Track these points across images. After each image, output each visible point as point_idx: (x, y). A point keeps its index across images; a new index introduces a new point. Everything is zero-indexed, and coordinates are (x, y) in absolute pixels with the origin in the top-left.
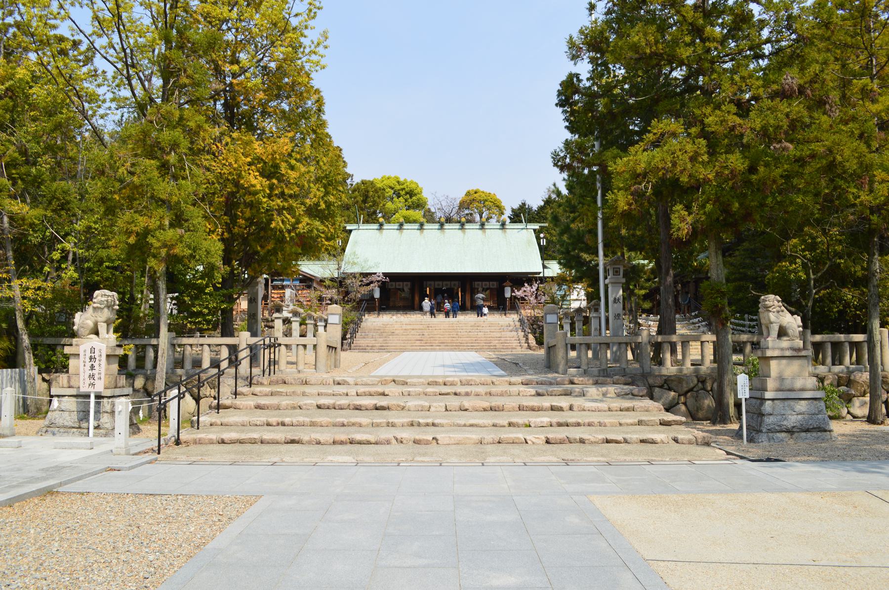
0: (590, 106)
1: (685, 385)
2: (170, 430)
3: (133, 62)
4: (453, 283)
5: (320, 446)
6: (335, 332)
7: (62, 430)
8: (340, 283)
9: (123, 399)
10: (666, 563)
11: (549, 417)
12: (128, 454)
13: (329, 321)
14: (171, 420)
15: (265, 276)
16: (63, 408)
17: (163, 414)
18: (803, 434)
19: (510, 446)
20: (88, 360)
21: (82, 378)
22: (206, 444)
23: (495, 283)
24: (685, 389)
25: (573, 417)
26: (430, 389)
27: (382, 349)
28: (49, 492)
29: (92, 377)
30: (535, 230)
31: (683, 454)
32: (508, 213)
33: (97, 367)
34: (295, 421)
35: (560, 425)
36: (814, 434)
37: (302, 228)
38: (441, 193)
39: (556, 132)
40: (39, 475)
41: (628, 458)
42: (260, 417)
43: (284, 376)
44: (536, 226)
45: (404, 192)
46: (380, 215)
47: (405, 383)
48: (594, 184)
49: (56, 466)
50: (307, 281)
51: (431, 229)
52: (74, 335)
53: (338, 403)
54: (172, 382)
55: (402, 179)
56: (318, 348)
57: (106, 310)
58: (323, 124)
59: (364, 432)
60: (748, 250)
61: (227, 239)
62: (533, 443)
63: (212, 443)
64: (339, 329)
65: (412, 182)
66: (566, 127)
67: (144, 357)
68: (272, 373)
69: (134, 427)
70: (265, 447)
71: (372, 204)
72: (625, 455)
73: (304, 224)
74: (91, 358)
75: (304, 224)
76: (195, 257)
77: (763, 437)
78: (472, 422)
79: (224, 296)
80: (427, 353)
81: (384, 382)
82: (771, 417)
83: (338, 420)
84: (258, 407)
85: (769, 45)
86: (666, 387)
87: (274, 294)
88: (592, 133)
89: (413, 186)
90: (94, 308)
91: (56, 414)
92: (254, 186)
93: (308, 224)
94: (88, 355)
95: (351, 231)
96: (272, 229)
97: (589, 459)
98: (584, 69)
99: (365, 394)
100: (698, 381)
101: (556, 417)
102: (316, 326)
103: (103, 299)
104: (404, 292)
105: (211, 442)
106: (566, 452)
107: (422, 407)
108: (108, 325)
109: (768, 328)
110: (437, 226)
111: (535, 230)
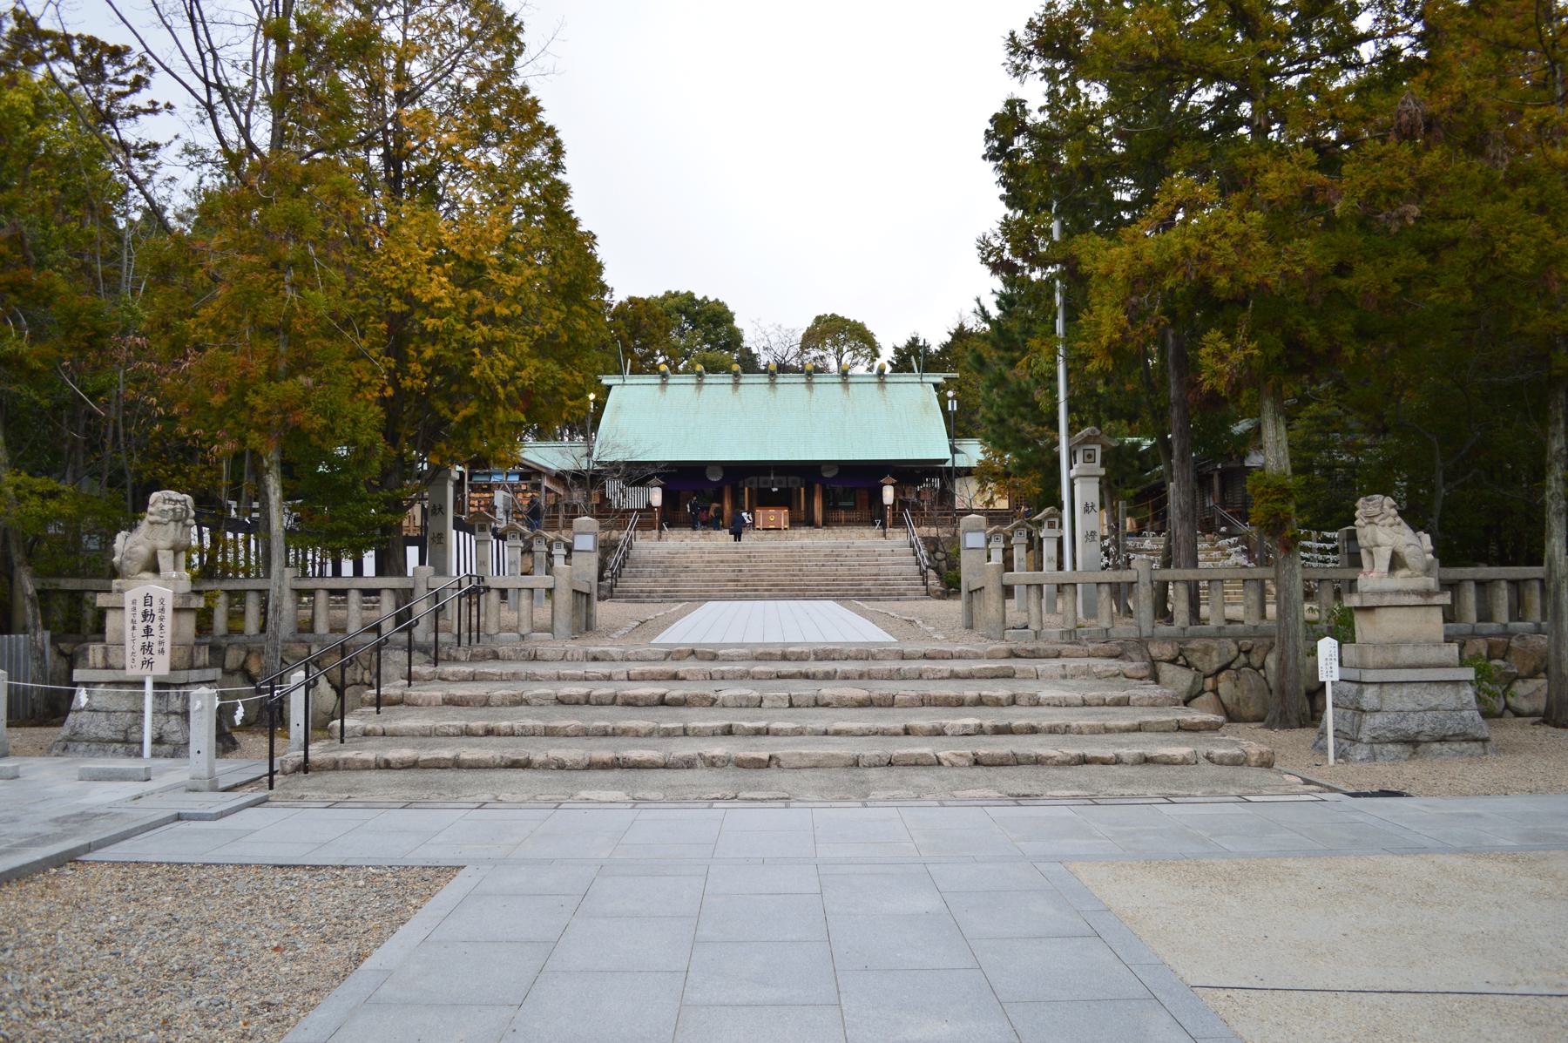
0: (1045, 155)
1: (1215, 659)
2: (291, 753)
3: (217, 78)
4: (791, 478)
5: (565, 773)
6: (587, 566)
7: (93, 746)
8: (590, 480)
9: (204, 690)
10: (1229, 992)
11: (977, 717)
12: (214, 789)
13: (576, 547)
14: (293, 725)
15: (459, 468)
16: (95, 705)
17: (277, 714)
18: (1436, 746)
19: (907, 770)
20: (139, 618)
21: (128, 651)
22: (357, 769)
24: (1216, 666)
25: (1021, 717)
26: (760, 668)
27: (670, 596)
28: (69, 859)
29: (147, 648)
30: (936, 386)
31: (1226, 783)
32: (887, 355)
33: (156, 631)
34: (517, 725)
35: (998, 731)
36: (1456, 746)
37: (527, 375)
38: (767, 324)
39: (984, 204)
40: (49, 829)
41: (1127, 792)
42: (454, 720)
43: (494, 646)
44: (939, 378)
46: (661, 359)
47: (714, 657)
48: (1051, 297)
49: (82, 814)
50: (531, 474)
51: (754, 386)
52: (115, 573)
53: (595, 693)
54: (293, 658)
56: (557, 595)
57: (172, 524)
58: (562, 191)
59: (644, 747)
60: (1316, 418)
61: (392, 399)
62: (953, 765)
63: (369, 768)
64: (594, 559)
66: (1002, 198)
67: (243, 613)
68: (474, 641)
69: (226, 741)
70: (466, 776)
72: (1122, 786)
73: (530, 369)
74: (145, 615)
75: (530, 369)
76: (332, 431)
77: (1361, 752)
78: (840, 725)
79: (387, 501)
81: (671, 655)
82: (1378, 716)
83: (597, 724)
84: (450, 702)
85: (1371, 43)
86: (1181, 660)
87: (474, 500)
88: (1049, 208)
90: (152, 523)
91: (84, 717)
92: (440, 300)
93: (537, 370)
94: (140, 608)
95: (609, 387)
96: (473, 380)
97: (1055, 793)
98: (1034, 92)
99: (643, 677)
100: (1240, 651)
101: (990, 717)
102: (550, 555)
103: (167, 507)
104: (703, 493)
105: (365, 766)
106: (1016, 779)
107: (749, 699)
108: (176, 554)
109: (1371, 553)
110: (764, 379)
111: (936, 386)
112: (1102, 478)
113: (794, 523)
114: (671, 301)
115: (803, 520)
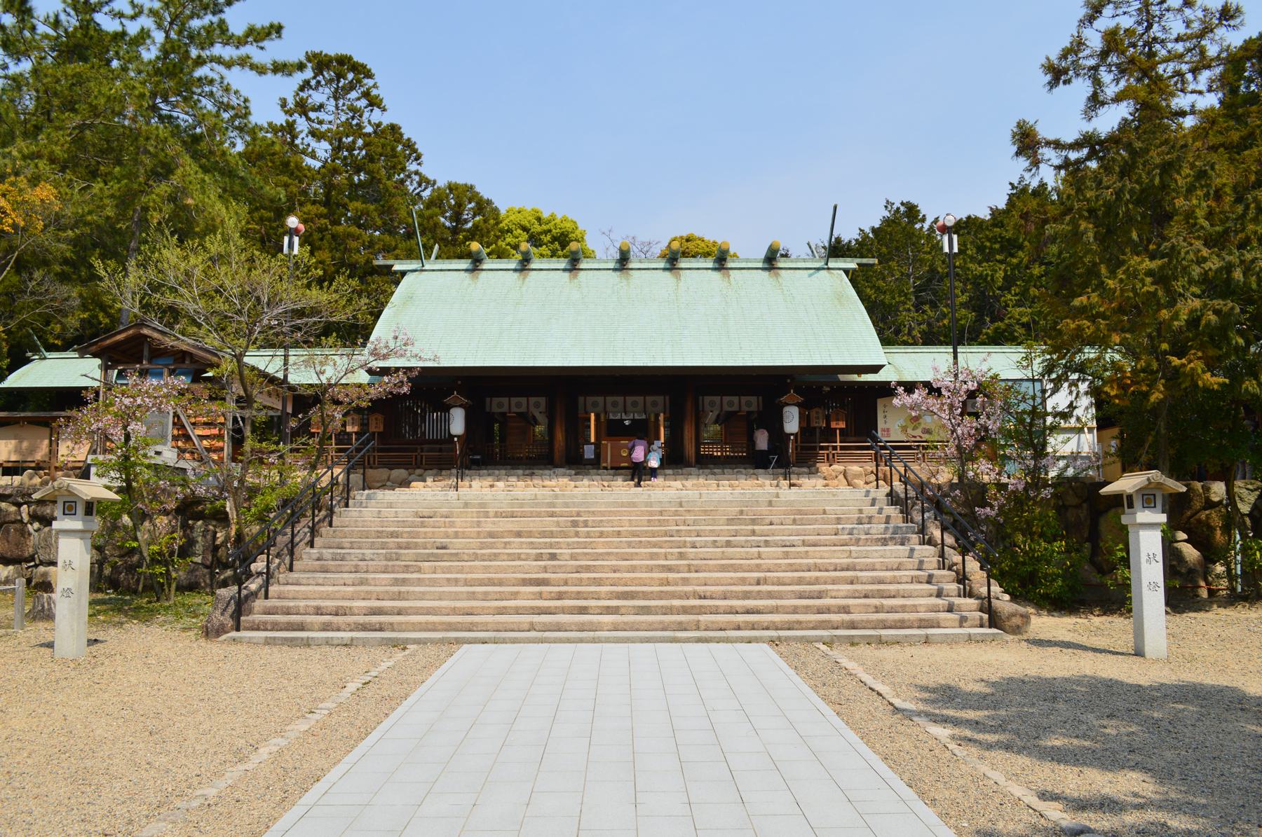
23: (753, 399)
45: (548, 238)
55: (545, 215)
65: (564, 220)
71: (466, 230)
80: (561, 653)
89: (568, 225)
95: (403, 273)
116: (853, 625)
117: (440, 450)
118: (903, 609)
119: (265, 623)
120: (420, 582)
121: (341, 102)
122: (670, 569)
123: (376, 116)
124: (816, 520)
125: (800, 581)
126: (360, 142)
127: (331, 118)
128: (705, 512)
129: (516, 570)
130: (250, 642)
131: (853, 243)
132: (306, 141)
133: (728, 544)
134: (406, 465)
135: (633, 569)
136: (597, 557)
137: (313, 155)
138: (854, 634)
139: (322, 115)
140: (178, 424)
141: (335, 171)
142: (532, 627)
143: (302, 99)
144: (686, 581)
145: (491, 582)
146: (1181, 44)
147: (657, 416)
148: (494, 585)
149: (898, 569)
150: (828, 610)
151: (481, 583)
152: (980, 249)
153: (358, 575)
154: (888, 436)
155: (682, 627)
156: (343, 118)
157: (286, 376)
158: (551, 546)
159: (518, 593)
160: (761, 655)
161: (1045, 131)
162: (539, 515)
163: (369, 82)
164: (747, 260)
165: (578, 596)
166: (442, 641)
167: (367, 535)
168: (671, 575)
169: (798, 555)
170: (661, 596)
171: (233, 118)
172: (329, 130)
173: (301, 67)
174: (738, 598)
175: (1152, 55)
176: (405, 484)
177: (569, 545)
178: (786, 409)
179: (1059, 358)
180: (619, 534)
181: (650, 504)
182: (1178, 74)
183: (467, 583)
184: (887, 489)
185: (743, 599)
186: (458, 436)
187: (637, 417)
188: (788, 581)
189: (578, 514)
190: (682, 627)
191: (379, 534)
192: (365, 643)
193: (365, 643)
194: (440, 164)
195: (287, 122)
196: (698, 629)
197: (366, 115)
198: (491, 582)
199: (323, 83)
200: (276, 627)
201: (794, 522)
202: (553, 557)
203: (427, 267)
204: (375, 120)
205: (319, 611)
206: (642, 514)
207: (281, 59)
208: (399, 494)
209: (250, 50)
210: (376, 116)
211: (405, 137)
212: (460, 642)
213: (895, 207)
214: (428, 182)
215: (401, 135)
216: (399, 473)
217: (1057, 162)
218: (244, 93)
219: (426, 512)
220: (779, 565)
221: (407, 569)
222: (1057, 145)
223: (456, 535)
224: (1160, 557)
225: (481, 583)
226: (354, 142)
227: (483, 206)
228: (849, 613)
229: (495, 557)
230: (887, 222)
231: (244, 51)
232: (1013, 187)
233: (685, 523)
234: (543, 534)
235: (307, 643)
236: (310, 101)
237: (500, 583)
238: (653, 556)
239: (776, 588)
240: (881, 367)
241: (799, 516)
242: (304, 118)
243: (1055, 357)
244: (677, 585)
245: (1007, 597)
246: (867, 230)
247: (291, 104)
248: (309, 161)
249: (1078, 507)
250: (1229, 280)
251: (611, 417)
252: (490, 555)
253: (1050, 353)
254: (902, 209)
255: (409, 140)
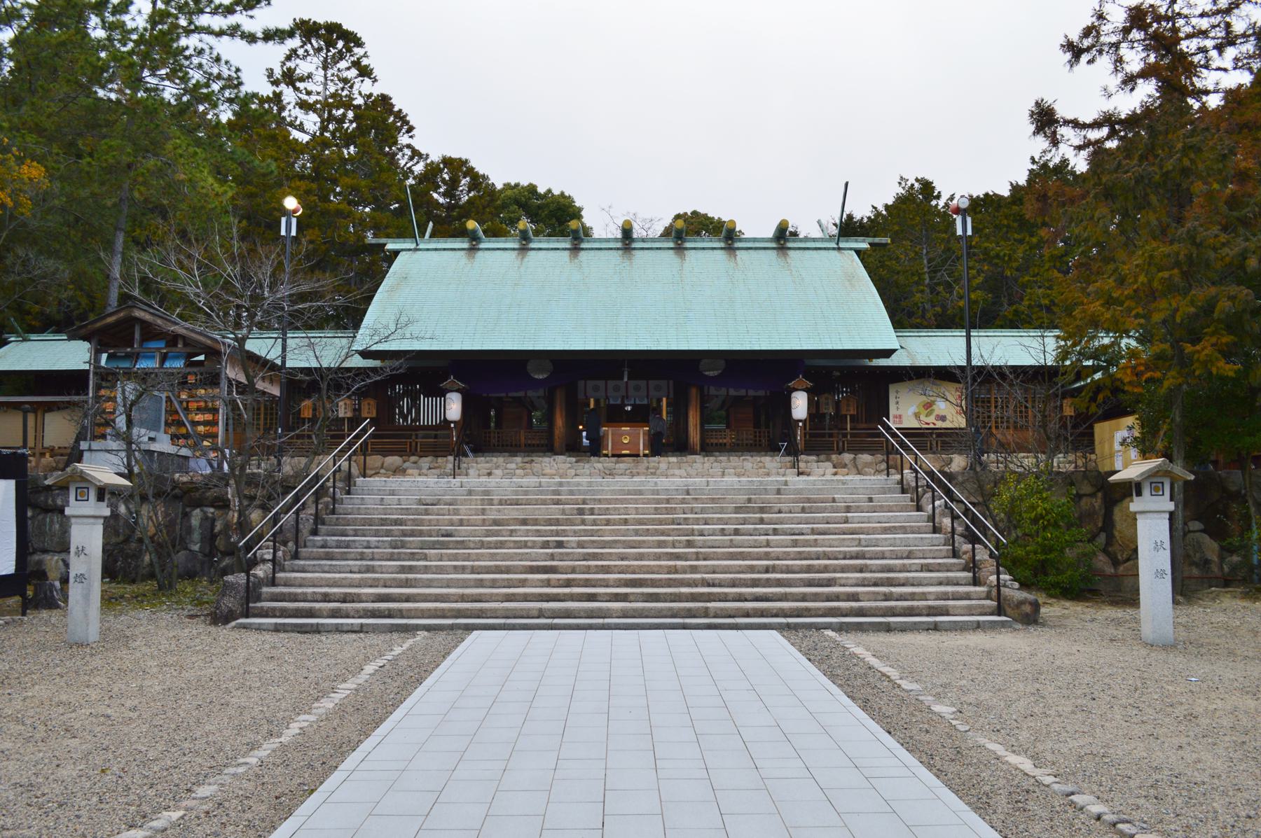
95: (396, 253)
112: (1171, 514)
113: (658, 447)
114: (509, 193)
115: (670, 443)
116: (861, 612)
117: (436, 437)
118: (912, 597)
119: (274, 609)
120: (426, 569)
121: (330, 72)
122: (677, 557)
123: (366, 87)
124: (825, 508)
125: (809, 569)
126: (350, 114)
127: (320, 89)
128: (713, 500)
129: (522, 557)
130: (259, 628)
131: (865, 220)
132: (294, 113)
133: (737, 532)
134: (400, 452)
135: (641, 557)
136: (604, 545)
137: (301, 128)
138: (860, 620)
139: (310, 86)
140: (172, 411)
141: (325, 144)
142: (541, 614)
143: (289, 69)
144: (694, 569)
145: (498, 570)
146: (1205, 19)
147: (659, 401)
148: (501, 572)
149: (908, 558)
150: (837, 598)
151: (488, 570)
152: (998, 227)
153: (365, 563)
154: (901, 422)
155: (691, 614)
156: (332, 89)
157: (284, 362)
158: (557, 534)
159: (526, 580)
160: (771, 645)
161: (1062, 112)
162: (544, 502)
163: (358, 51)
164: (755, 240)
165: (587, 583)
166: (452, 627)
167: (370, 522)
168: (679, 563)
169: (807, 544)
170: (669, 583)
171: (223, 88)
172: (317, 102)
173: (291, 34)
174: (747, 586)
175: (1175, 30)
176: (398, 471)
177: (575, 533)
178: (794, 394)
179: (1074, 345)
180: (626, 522)
181: (657, 492)
182: (1203, 50)
183: (474, 570)
184: (898, 477)
185: (753, 586)
186: (455, 422)
187: (638, 402)
188: (796, 569)
189: (584, 502)
190: (691, 614)
191: (383, 522)
192: (375, 629)
193: (375, 629)
194: (431, 138)
195: (274, 92)
196: (706, 616)
197: (356, 87)
198: (498, 570)
199: (311, 52)
200: (284, 613)
201: (803, 510)
202: (560, 545)
203: (421, 246)
204: (366, 91)
205: (326, 598)
206: (649, 502)
207: (272, 26)
208: (394, 482)
209: (239, 18)
210: (366, 87)
211: (396, 109)
212: (470, 628)
213: (909, 183)
214: (420, 155)
215: (393, 106)
216: (393, 460)
217: (1077, 142)
218: (235, 63)
219: (429, 499)
220: (788, 553)
221: (412, 557)
222: (1076, 124)
223: (461, 523)
224: (1167, 545)
225: (488, 570)
226: (344, 115)
227: (478, 181)
228: (858, 600)
229: (501, 545)
230: (900, 200)
231: (232, 20)
232: (1033, 161)
233: (692, 511)
234: (549, 522)
235: (317, 630)
236: (298, 71)
237: (508, 570)
238: (661, 544)
239: (785, 576)
240: (894, 351)
241: (808, 504)
242: (291, 89)
243: (1069, 343)
244: (685, 572)
245: (1016, 585)
246: (881, 208)
247: (278, 73)
248: (295, 134)
249: (1093, 495)
250: (1242, 266)
251: (612, 402)
252: (497, 542)
253: (1065, 339)
254: (917, 185)
255: (400, 111)
